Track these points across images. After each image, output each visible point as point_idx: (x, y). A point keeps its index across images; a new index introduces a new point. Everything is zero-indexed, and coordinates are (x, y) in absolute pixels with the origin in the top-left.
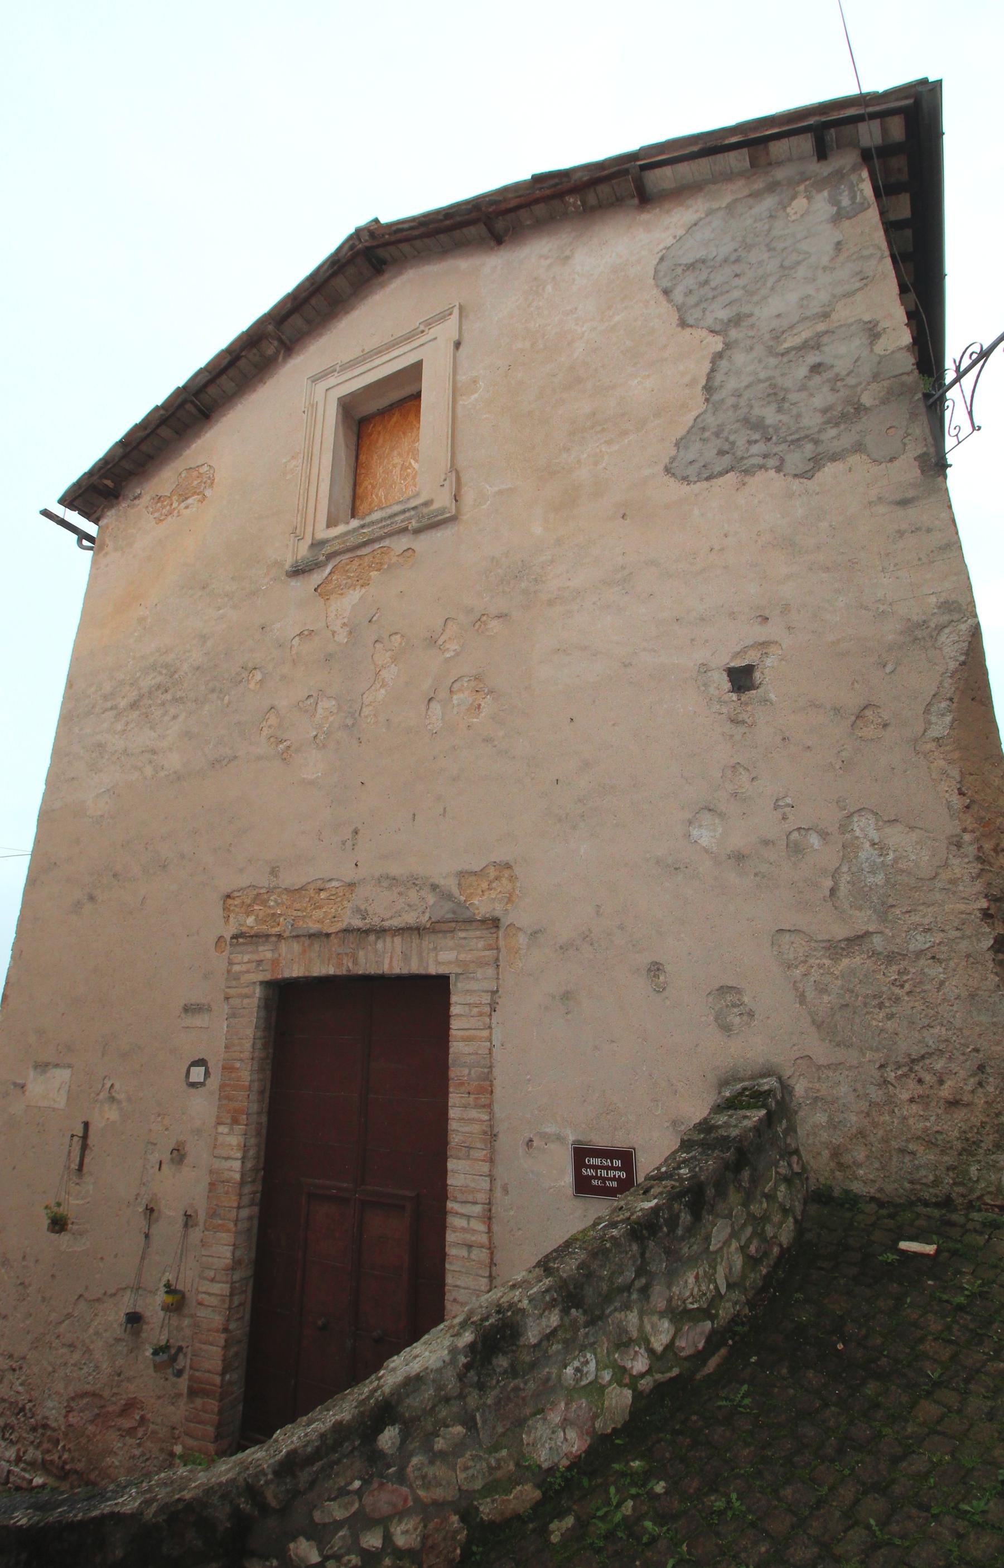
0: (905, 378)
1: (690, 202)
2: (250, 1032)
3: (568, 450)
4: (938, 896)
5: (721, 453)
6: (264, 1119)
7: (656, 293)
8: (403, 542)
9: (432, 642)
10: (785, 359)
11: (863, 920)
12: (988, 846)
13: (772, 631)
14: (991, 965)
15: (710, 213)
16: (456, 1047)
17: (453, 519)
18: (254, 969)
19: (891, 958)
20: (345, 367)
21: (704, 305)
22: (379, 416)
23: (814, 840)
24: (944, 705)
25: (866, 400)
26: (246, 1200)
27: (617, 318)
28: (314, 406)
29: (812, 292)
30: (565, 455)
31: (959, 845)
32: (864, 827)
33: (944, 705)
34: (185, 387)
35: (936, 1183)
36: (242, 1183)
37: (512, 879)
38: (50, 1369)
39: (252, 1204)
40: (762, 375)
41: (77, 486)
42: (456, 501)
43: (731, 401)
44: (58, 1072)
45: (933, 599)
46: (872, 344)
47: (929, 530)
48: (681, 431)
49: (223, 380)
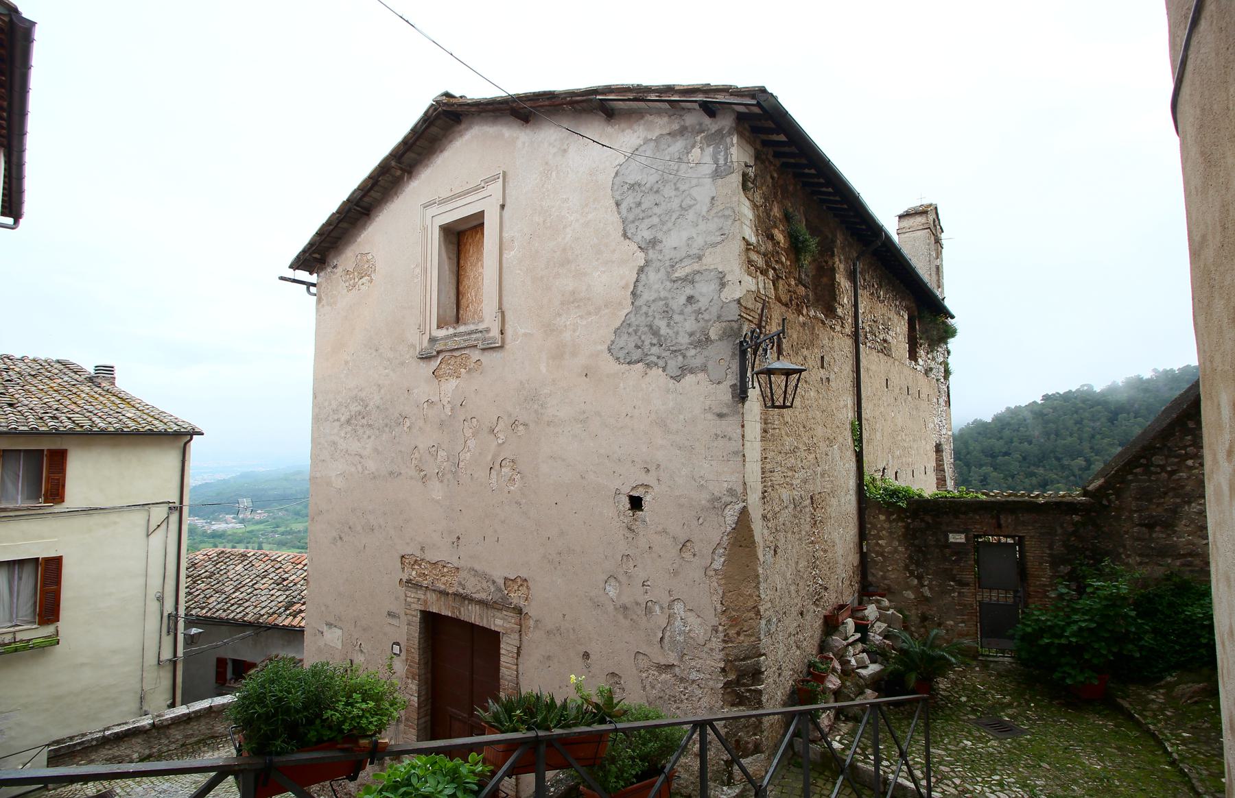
1: (636, 127)
3: (560, 315)
4: (705, 655)
6: (429, 675)
8: (475, 355)
10: (675, 286)
11: (672, 658)
15: (646, 141)
16: (503, 670)
17: (502, 347)
18: (418, 601)
19: (682, 680)
20: (443, 202)
21: (637, 223)
22: (461, 237)
23: (657, 608)
25: (713, 336)
35: (687, 787)
36: (419, 708)
37: (528, 587)
40: (663, 294)
41: (298, 257)
45: (725, 485)
46: (720, 291)
48: (618, 324)
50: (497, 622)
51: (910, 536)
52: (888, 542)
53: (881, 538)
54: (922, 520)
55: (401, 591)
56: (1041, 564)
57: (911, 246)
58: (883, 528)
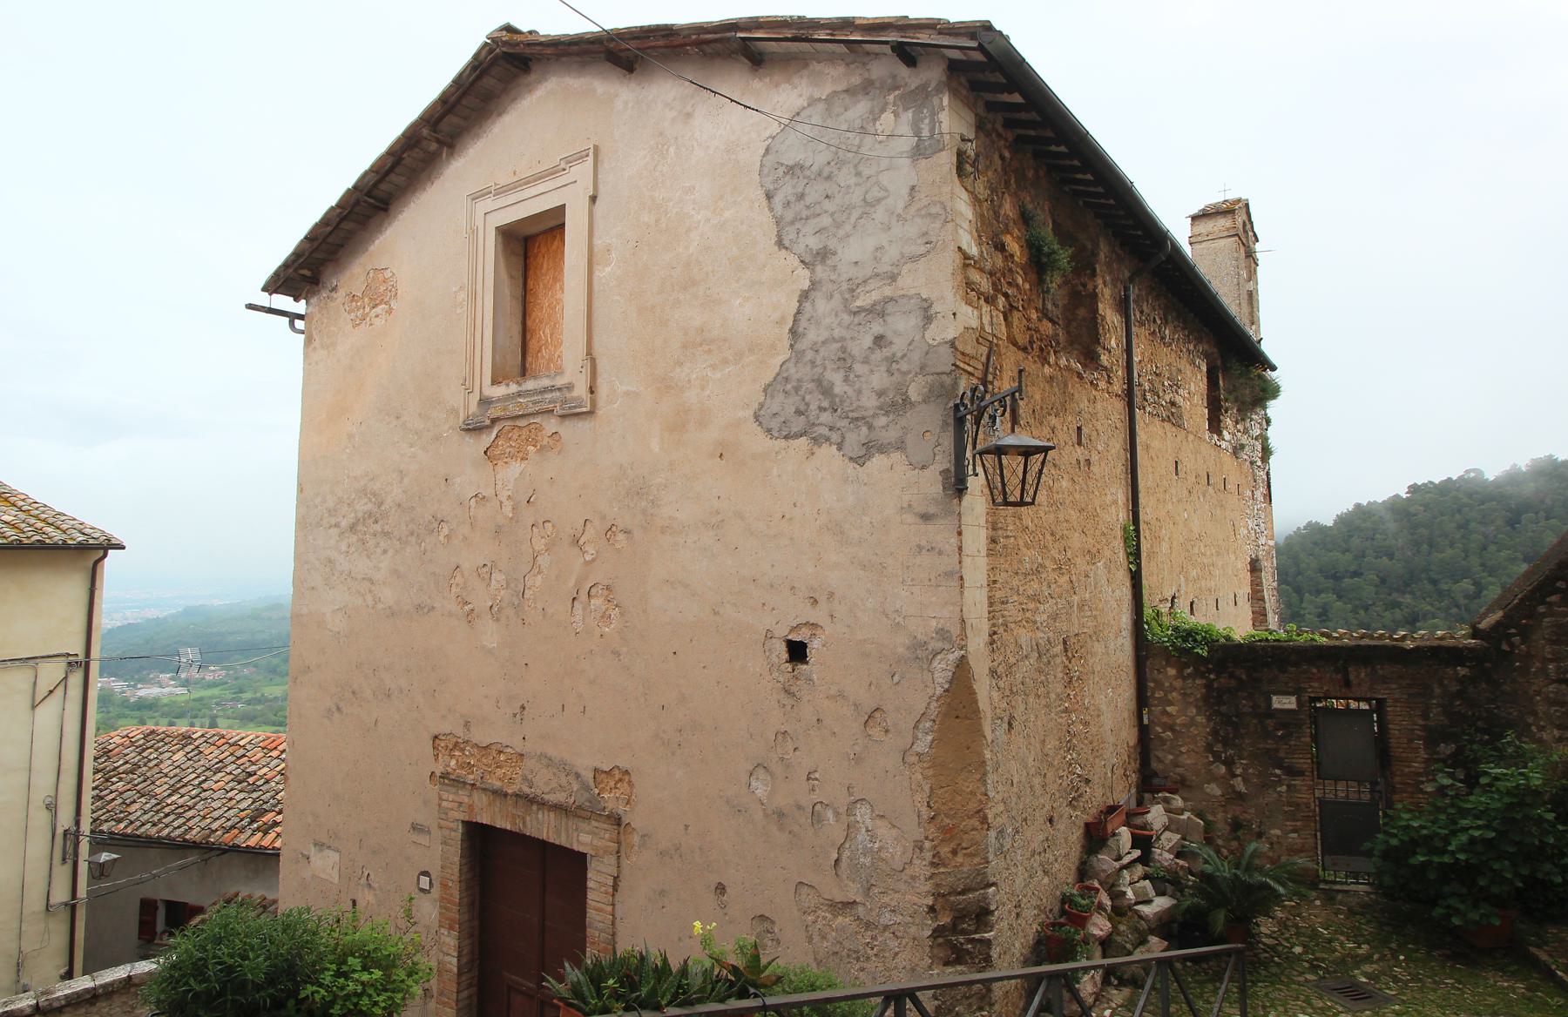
0: (944, 377)
1: (796, 80)
2: (457, 859)
4: (902, 886)
5: (799, 413)
6: (476, 923)
7: (760, 194)
8: (550, 425)
9: (576, 541)
11: (853, 892)
12: (945, 850)
13: (818, 615)
14: (928, 949)
15: (813, 102)
16: (591, 914)
19: (868, 925)
20: (502, 191)
21: (798, 225)
23: (830, 814)
24: (928, 724)
25: (914, 395)
26: (464, 985)
27: (727, 214)
28: (475, 231)
29: (885, 243)
30: (678, 370)
31: (921, 849)
32: (863, 814)
33: (928, 724)
34: (355, 187)
36: (460, 974)
38: (866, 172)
39: (470, 986)
40: (837, 333)
41: (277, 274)
42: (592, 392)
43: (810, 355)
44: (331, 853)
45: (934, 623)
46: (925, 328)
47: (940, 553)
49: (393, 177)
50: (582, 838)
51: (1213, 700)
52: (1182, 708)
53: (1171, 703)
54: (1232, 676)
55: (433, 790)
56: (1411, 741)
57: (1211, 263)
58: (1173, 689)
